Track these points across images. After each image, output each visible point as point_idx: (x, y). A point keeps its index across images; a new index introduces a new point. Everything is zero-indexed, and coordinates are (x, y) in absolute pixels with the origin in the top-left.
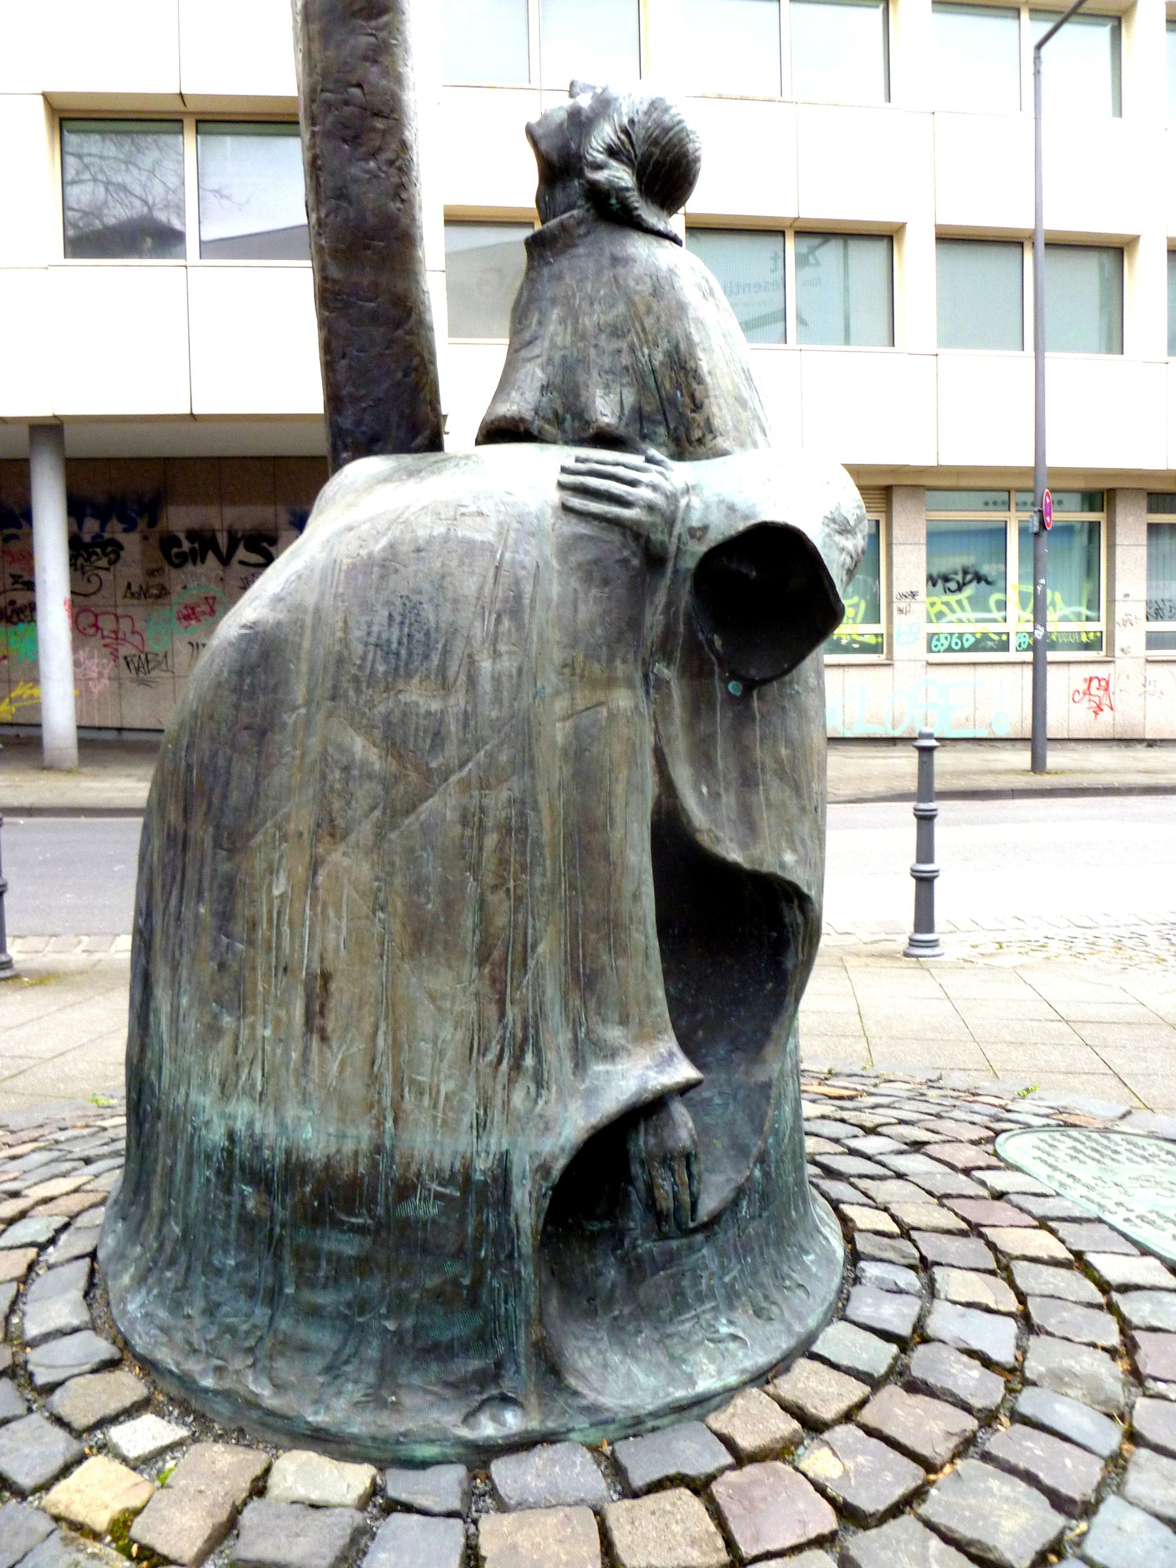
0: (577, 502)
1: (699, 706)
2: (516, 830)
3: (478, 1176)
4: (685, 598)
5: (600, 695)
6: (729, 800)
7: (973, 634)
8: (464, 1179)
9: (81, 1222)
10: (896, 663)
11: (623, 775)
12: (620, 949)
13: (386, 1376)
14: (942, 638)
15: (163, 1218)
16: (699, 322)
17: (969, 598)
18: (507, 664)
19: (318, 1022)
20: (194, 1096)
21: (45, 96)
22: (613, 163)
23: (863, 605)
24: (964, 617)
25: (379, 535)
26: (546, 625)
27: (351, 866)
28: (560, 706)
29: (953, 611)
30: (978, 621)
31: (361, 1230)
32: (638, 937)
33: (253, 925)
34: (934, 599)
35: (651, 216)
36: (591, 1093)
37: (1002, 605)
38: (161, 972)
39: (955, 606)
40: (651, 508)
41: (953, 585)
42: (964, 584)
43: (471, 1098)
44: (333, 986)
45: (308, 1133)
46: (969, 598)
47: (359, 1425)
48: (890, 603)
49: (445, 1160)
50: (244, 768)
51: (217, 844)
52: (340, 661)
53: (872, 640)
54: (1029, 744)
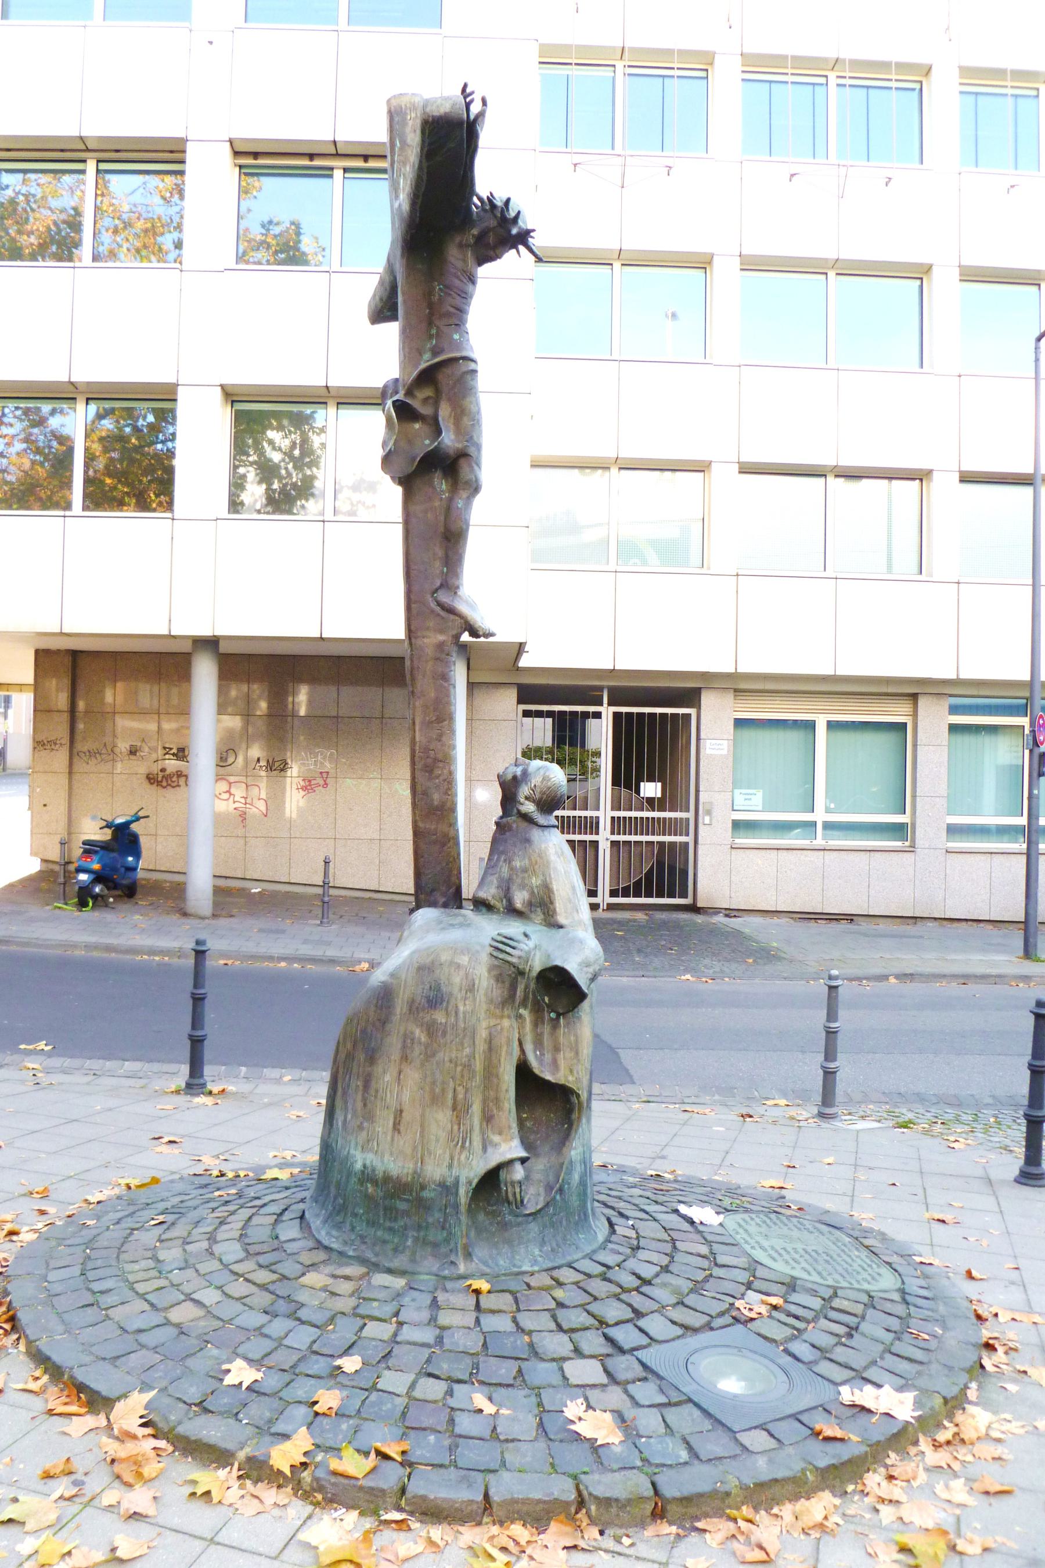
0: (495, 953)
1: (537, 1023)
2: (468, 1066)
4: (532, 985)
5: (498, 1021)
6: (548, 1057)
8: (442, 1185)
9: (292, 1207)
11: (504, 1049)
12: (499, 1108)
15: (335, 1198)
16: (555, 869)
18: (468, 1008)
20: (352, 1152)
21: (222, 386)
22: (527, 802)
26: (481, 996)
27: (413, 1076)
28: (484, 1024)
31: (407, 1200)
32: (506, 1105)
33: (377, 1091)
35: (541, 819)
38: (339, 1103)
40: (519, 957)
43: (447, 1156)
44: (404, 1114)
45: (392, 1165)
49: (437, 1177)
52: (413, 1001)
54: (1022, 926)
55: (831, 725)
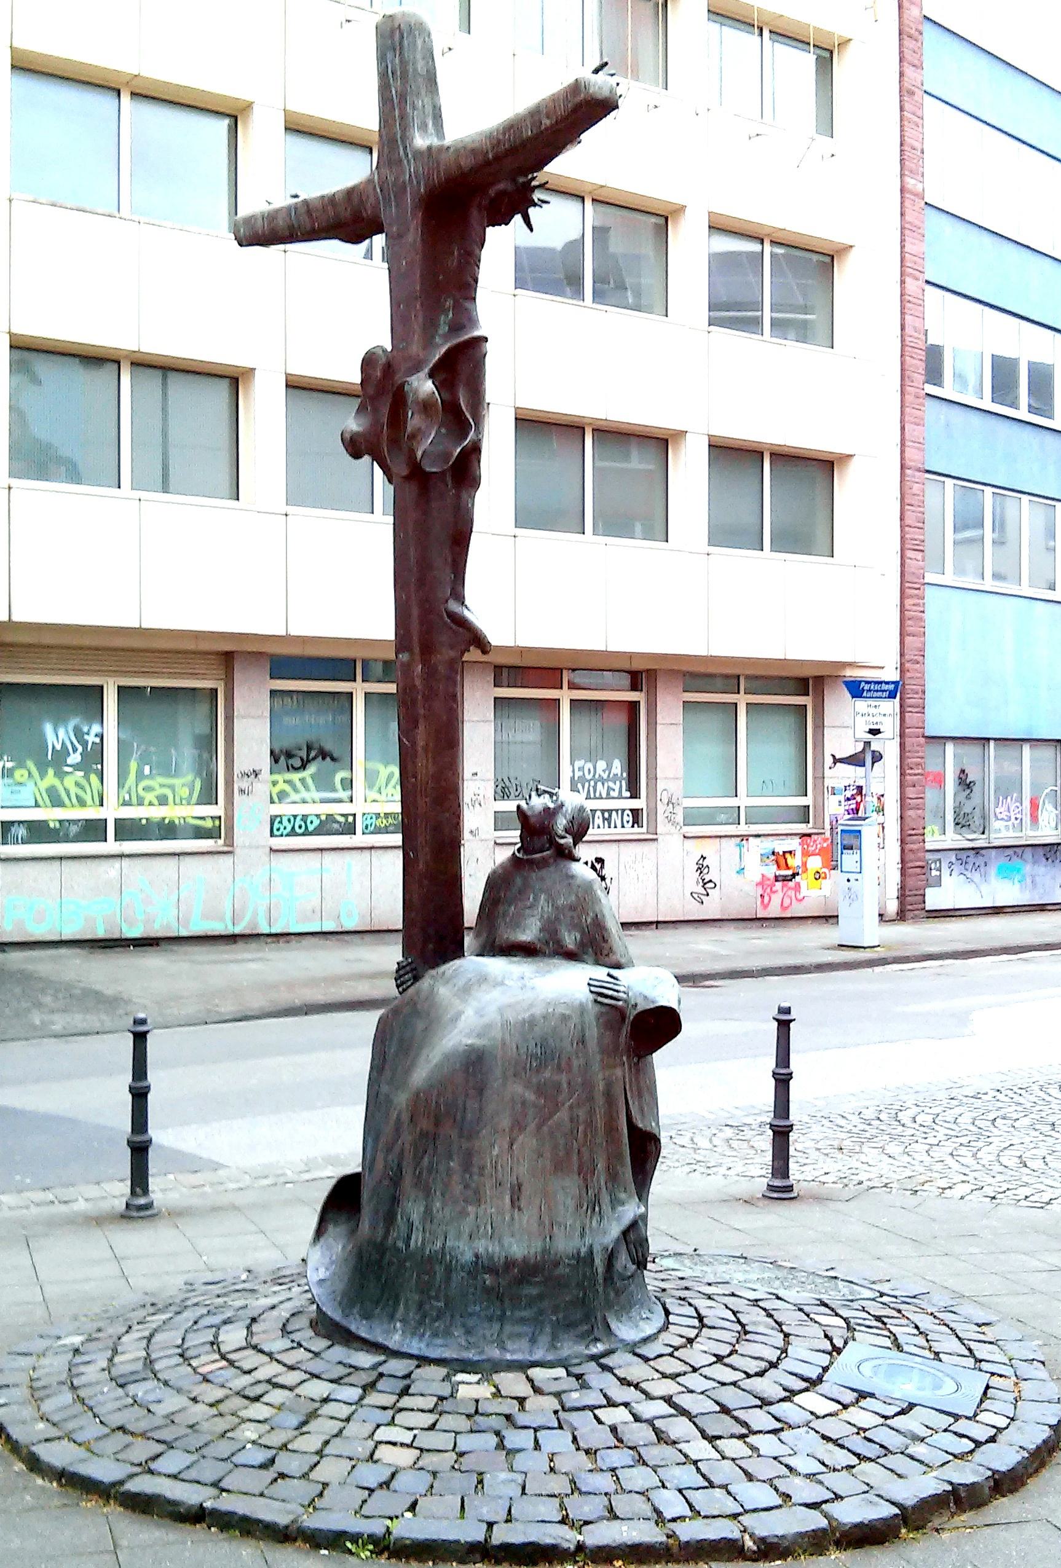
0: (600, 999)
3: (582, 1254)
7: (318, 816)
8: (577, 1257)
10: (238, 851)
13: (554, 1337)
14: (285, 820)
17: (312, 776)
19: (517, 1203)
23: (198, 785)
24: (307, 798)
25: (525, 1011)
26: (592, 1044)
27: (527, 1141)
28: (600, 1076)
29: (296, 790)
30: (323, 801)
33: (482, 1168)
34: (276, 777)
36: (619, 1219)
37: (349, 784)
39: (299, 784)
40: (625, 1001)
41: (297, 763)
42: (308, 761)
43: (578, 1225)
44: (523, 1188)
45: (515, 1248)
46: (312, 776)
47: (550, 1357)
48: (229, 783)
50: (472, 1104)
51: (461, 1136)
53: (209, 824)
55: (121, 690)
